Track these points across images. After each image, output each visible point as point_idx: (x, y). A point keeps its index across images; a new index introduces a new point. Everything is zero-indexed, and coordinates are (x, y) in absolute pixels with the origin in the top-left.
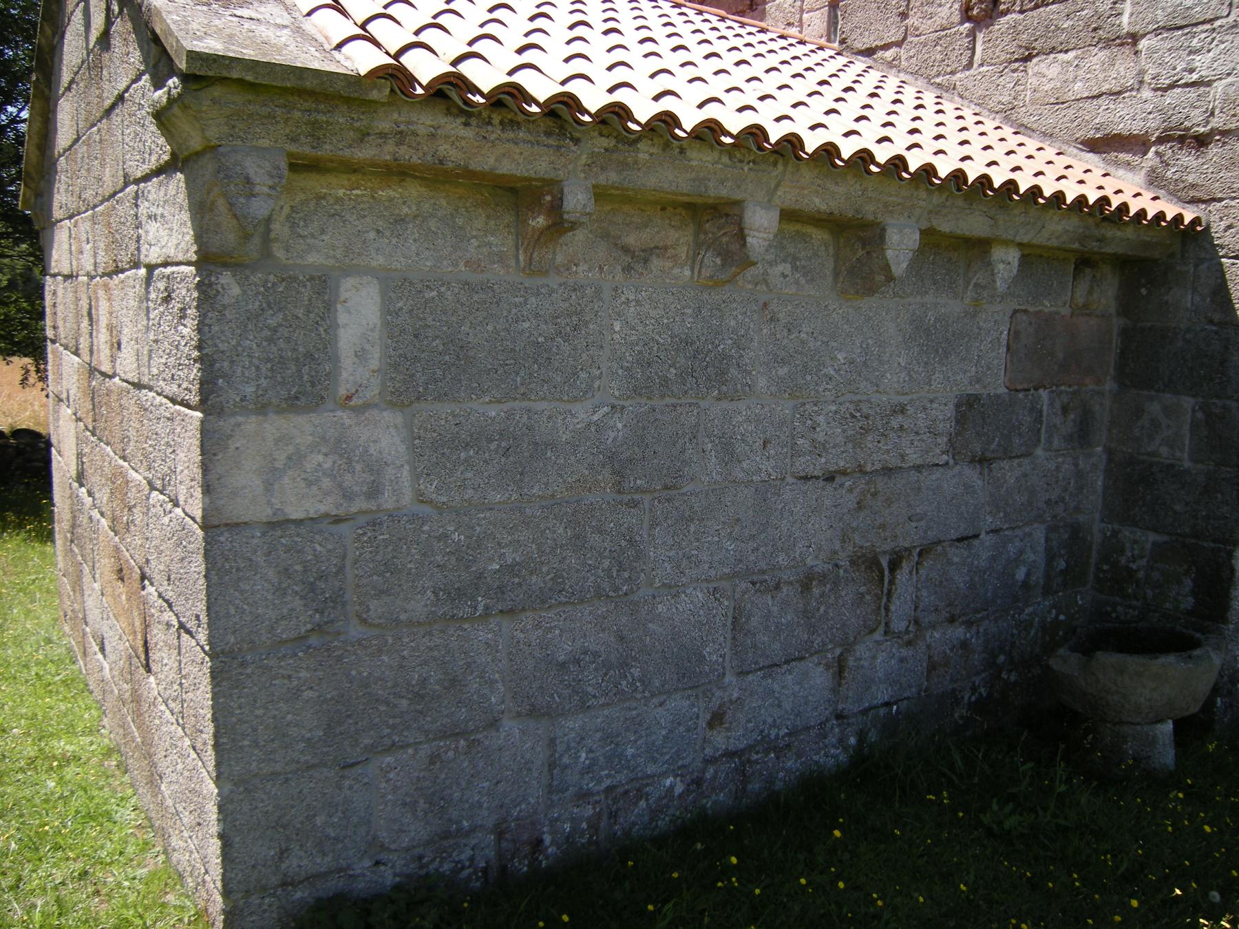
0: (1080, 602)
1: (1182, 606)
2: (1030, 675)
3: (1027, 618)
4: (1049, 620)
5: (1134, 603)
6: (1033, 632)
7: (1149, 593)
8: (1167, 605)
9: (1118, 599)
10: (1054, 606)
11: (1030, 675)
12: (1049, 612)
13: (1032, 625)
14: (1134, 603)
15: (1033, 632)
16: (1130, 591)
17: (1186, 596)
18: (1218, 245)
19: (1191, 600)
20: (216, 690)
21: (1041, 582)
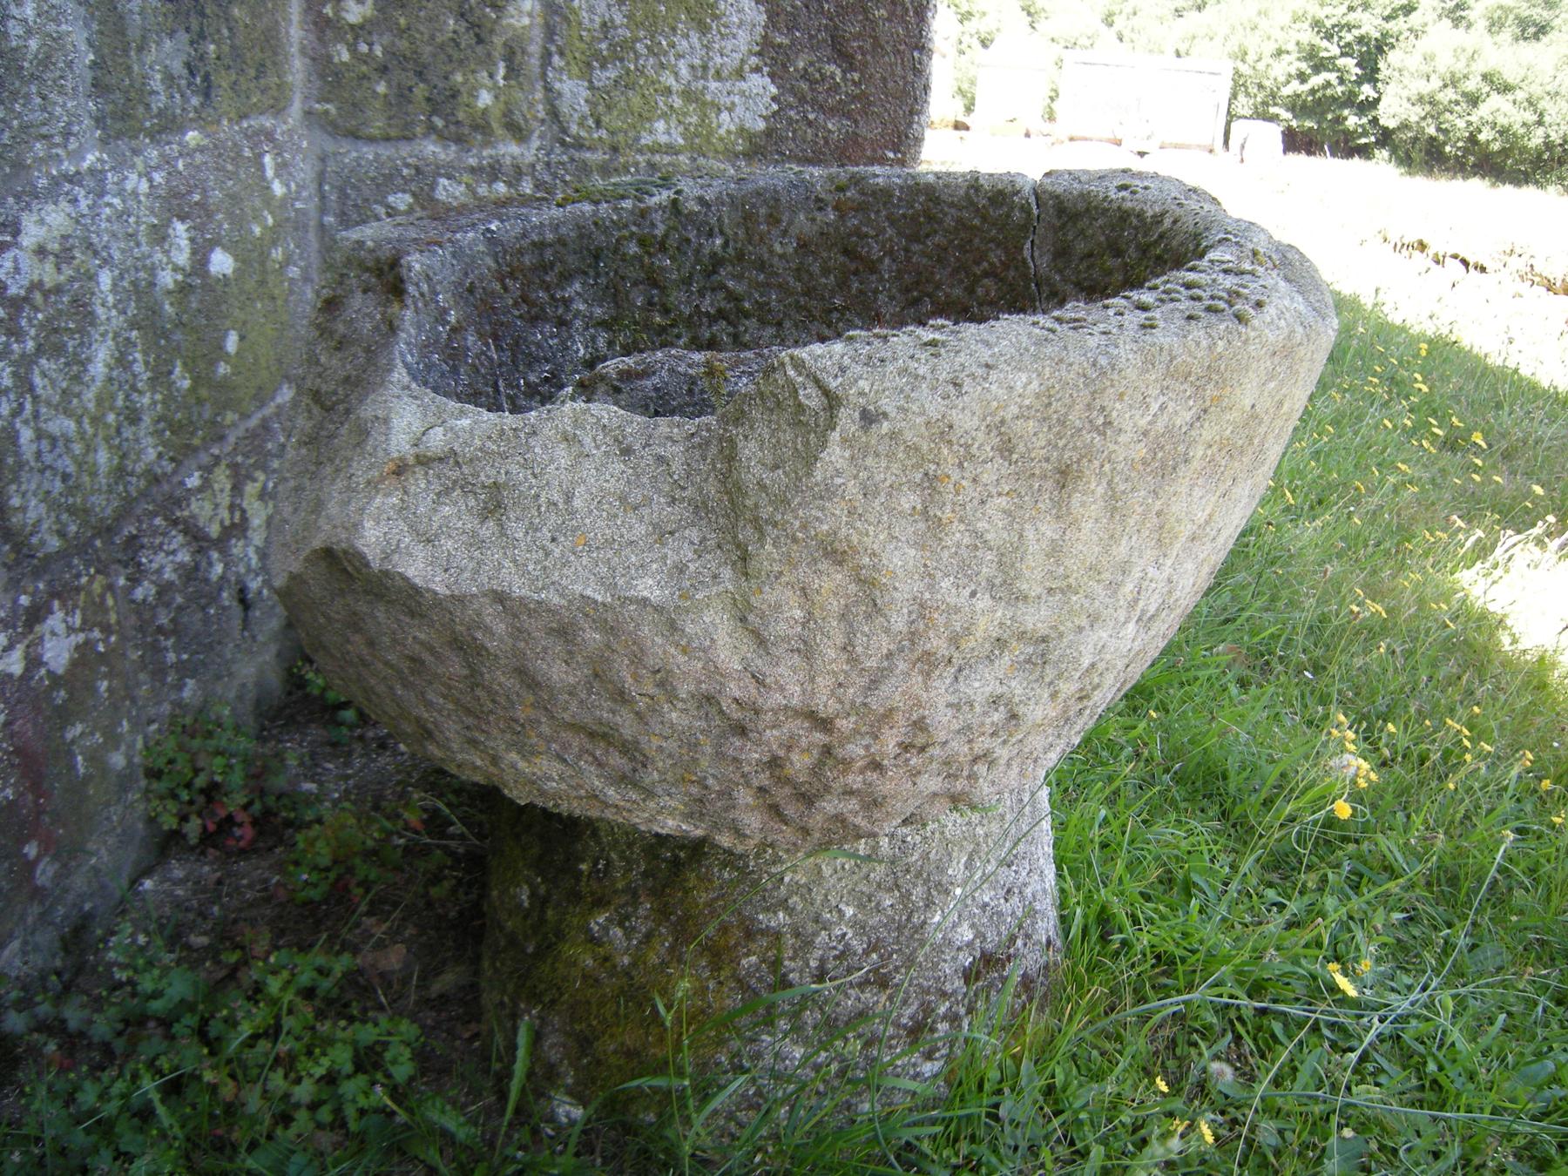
0: (278, 189)
1: (726, 123)
2: (142, 592)
3: (49, 274)
4: (167, 279)
5: (510, 150)
6: (101, 357)
7: (573, 92)
8: (661, 131)
9: (431, 149)
10: (175, 204)
11: (142, 592)
12: (160, 236)
13: (82, 309)
14: (510, 150)
15: (101, 357)
16: (485, 99)
17: (739, 74)
18: (156, 216)
19: (761, 85)
20: (888, 310)
21: (84, 1108)
